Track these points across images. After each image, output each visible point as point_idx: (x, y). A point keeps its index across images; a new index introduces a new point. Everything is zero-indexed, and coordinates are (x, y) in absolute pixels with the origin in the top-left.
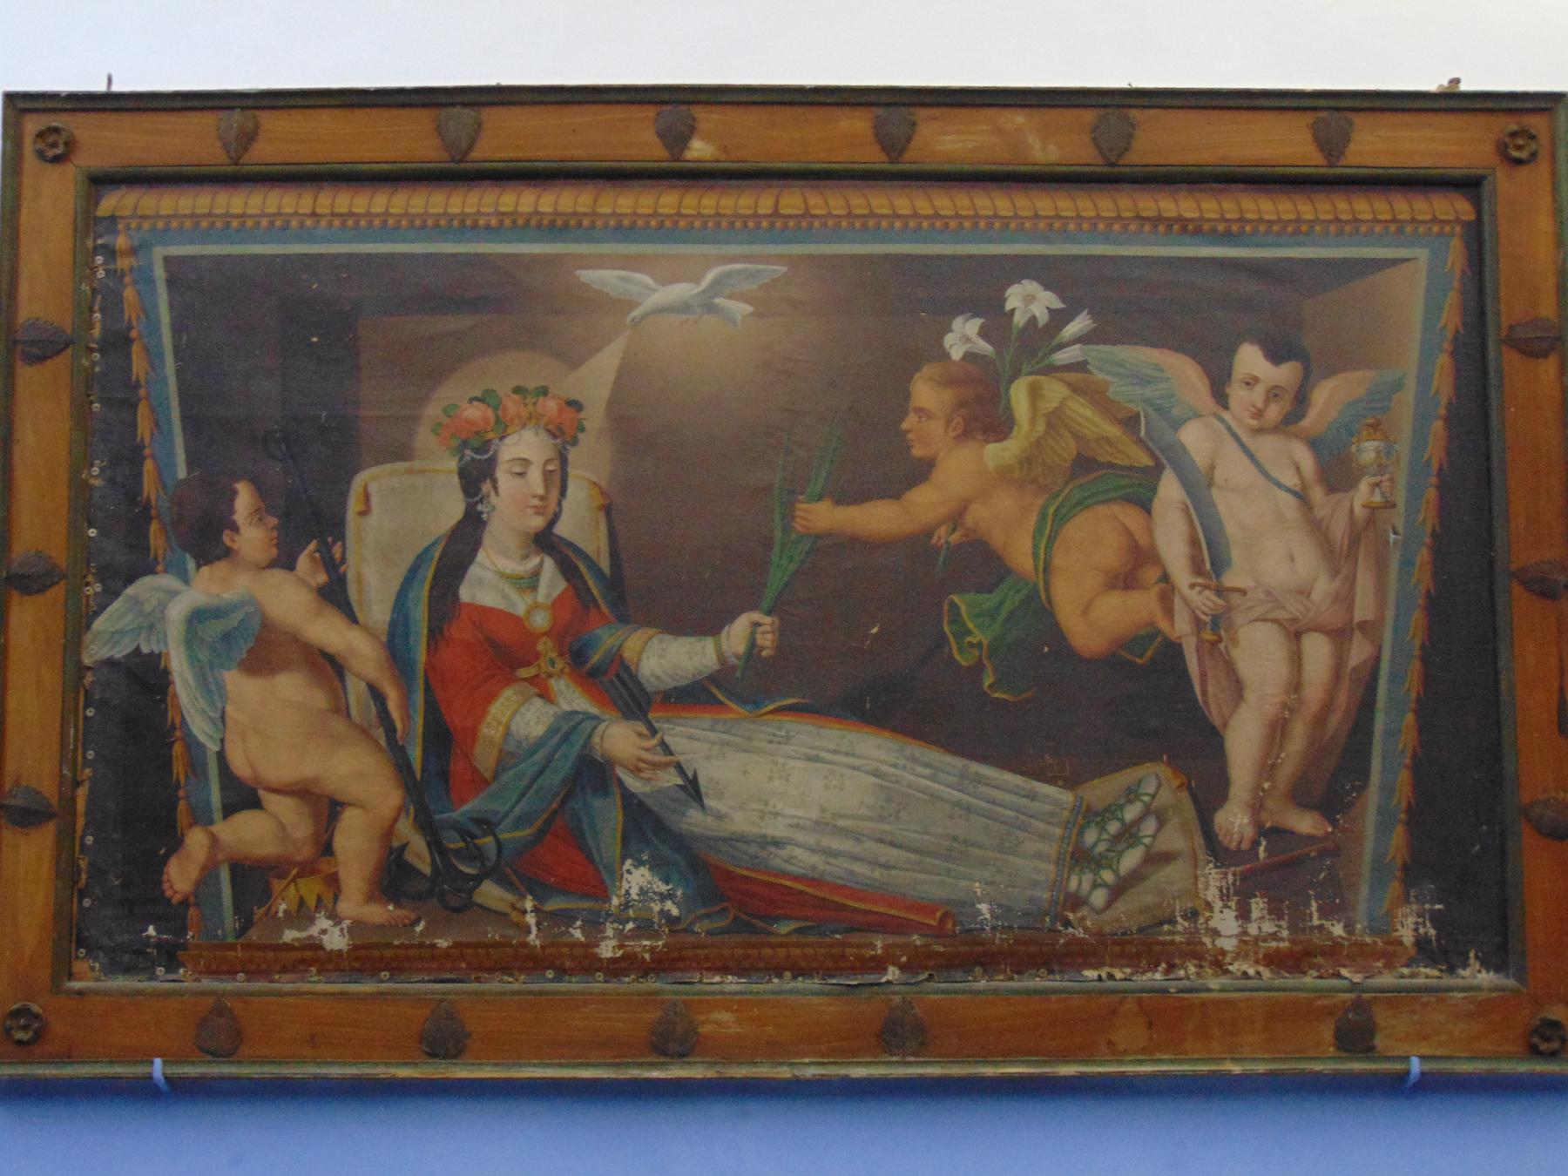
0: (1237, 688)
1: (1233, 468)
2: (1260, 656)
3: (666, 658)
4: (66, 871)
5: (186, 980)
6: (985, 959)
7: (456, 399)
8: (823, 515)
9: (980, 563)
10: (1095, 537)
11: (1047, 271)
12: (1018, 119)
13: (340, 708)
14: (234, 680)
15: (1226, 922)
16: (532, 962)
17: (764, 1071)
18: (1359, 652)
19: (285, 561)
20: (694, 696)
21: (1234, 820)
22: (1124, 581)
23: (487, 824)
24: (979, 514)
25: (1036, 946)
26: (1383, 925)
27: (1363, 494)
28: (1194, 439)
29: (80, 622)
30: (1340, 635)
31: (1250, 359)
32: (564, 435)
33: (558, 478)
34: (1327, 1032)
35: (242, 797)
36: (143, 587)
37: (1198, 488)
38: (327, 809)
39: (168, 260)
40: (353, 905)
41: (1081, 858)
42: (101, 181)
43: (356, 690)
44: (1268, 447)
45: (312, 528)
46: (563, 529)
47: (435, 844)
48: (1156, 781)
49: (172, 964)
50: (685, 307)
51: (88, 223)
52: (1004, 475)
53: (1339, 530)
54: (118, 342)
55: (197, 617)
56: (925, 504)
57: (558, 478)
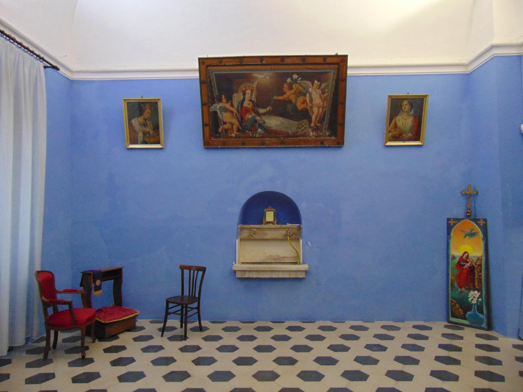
0: (313, 113)
1: (314, 92)
2: (315, 110)
3: (262, 111)
4: (210, 130)
5: (221, 139)
6: (290, 137)
7: (242, 87)
8: (276, 98)
9: (290, 102)
10: (301, 99)
11: (297, 73)
12: (294, 58)
13: (233, 116)
14: (223, 113)
15: (311, 133)
16: (251, 137)
17: (271, 146)
18: (324, 109)
19: (227, 102)
20: (264, 114)
21: (312, 125)
22: (303, 103)
23: (246, 126)
24: (290, 97)
25: (295, 135)
26: (325, 134)
27: (326, 95)
28: (310, 90)
29: (209, 108)
30: (323, 108)
31: (316, 82)
32: (252, 91)
33: (252, 95)
34: (320, 142)
35: (225, 123)
36: (215, 105)
37: (310, 94)
38: (232, 124)
39: (215, 75)
40: (235, 132)
41: (299, 128)
42: (208, 66)
43: (234, 114)
44: (317, 90)
45: (229, 99)
46: (252, 99)
47: (242, 127)
48: (306, 121)
49: (220, 138)
50: (263, 78)
51: (207, 70)
52: (292, 94)
53: (323, 98)
54: (211, 82)
55: (220, 108)
56: (285, 96)
57: (252, 95)
